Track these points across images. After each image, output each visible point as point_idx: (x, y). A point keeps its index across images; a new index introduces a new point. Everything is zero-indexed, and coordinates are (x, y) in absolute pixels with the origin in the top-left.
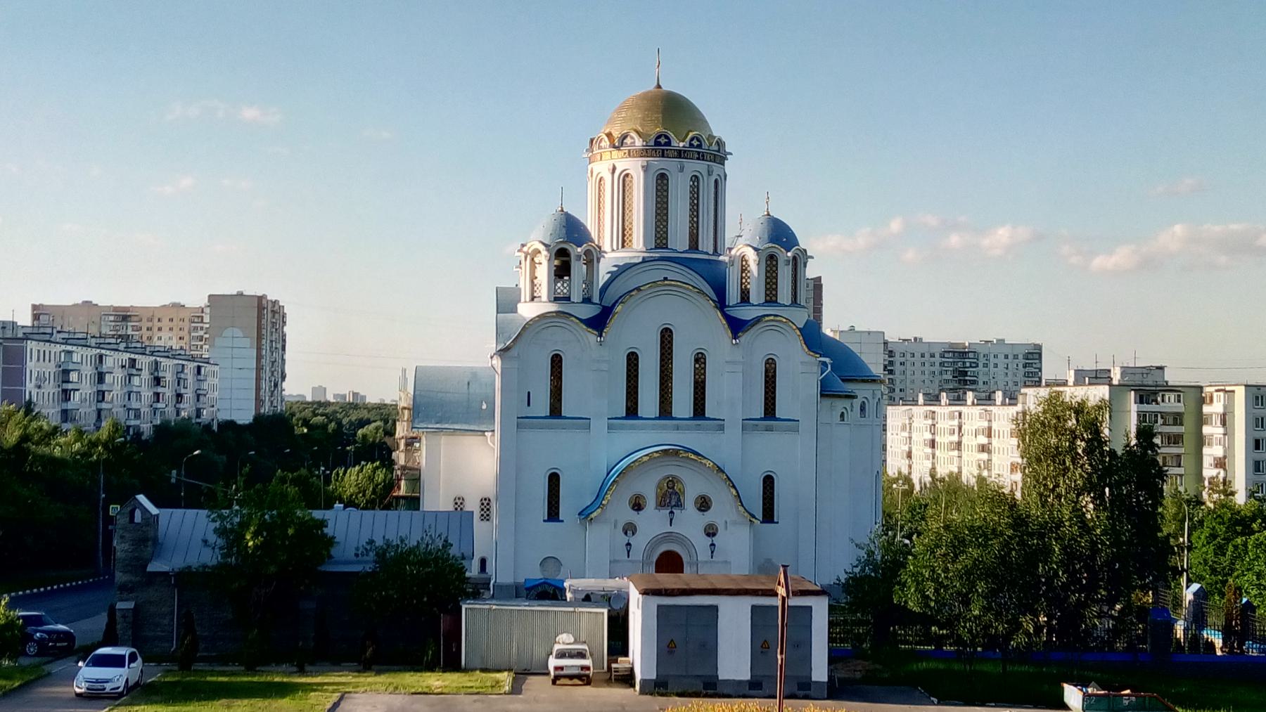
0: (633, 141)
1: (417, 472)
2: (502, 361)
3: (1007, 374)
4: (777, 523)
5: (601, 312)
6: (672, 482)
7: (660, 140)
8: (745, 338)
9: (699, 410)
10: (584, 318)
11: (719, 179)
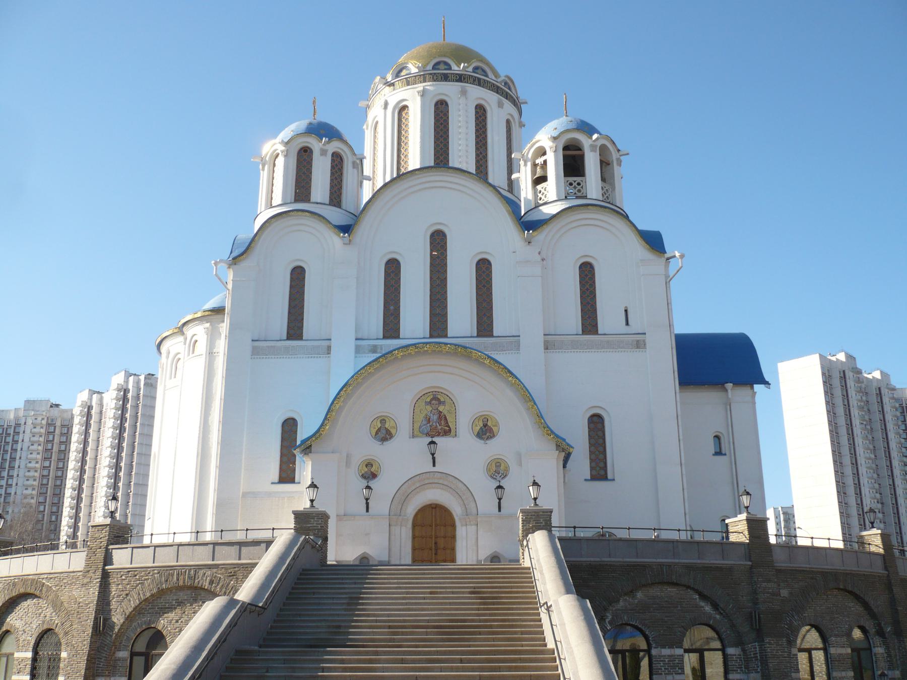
1: (56, 549)
2: (233, 271)
3: (481, 171)
5: (852, 633)
6: (435, 399)
9: (485, 325)
10: (337, 224)
11: (512, 121)
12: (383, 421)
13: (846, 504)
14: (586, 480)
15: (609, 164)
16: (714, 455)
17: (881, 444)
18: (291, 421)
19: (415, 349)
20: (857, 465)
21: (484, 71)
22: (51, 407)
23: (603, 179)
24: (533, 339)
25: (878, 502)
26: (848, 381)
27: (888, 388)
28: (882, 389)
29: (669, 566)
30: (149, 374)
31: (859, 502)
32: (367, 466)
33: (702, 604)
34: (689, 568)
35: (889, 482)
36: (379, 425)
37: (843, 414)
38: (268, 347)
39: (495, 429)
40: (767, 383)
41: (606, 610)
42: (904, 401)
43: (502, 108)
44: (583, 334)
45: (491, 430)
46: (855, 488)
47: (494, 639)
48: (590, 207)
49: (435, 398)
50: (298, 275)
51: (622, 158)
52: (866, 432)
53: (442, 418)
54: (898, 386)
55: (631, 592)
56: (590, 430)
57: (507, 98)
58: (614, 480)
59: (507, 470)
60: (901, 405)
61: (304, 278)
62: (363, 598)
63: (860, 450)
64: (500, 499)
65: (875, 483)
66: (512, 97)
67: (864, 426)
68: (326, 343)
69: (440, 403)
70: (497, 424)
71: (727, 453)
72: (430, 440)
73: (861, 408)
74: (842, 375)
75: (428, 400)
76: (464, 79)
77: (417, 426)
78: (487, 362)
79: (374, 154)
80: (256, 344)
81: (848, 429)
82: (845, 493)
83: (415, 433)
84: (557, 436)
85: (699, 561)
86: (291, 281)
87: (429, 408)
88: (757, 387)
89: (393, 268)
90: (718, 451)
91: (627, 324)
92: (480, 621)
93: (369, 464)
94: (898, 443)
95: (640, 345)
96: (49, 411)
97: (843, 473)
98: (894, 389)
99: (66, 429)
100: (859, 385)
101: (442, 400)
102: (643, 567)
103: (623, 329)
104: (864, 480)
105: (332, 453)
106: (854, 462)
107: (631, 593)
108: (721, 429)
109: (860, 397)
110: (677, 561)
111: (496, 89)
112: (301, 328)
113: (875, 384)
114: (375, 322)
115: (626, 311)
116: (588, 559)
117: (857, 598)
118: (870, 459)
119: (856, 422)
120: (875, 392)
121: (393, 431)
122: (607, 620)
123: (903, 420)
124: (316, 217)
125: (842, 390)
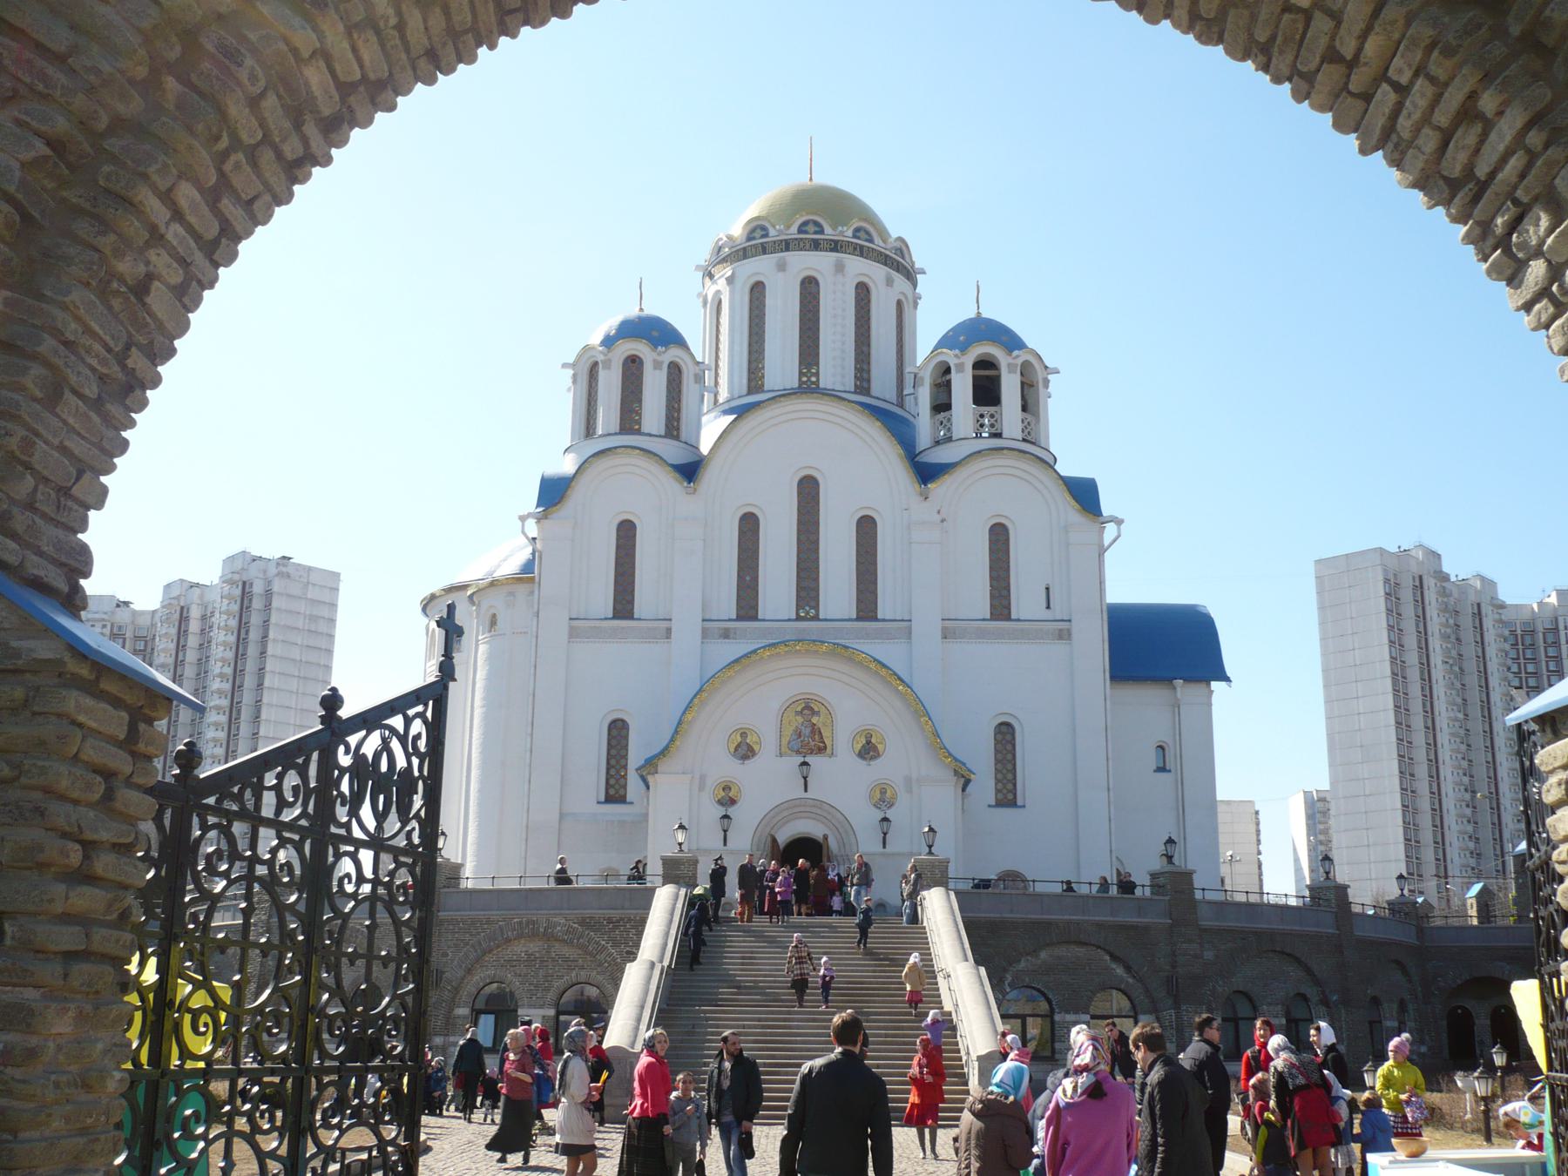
0: (764, 233)
4: (1024, 806)
6: (808, 708)
7: (807, 228)
8: (938, 488)
9: (867, 607)
10: (675, 463)
11: (904, 300)
12: (744, 735)
13: (1412, 792)
14: (989, 806)
15: (1033, 386)
16: (1155, 771)
17: (1475, 696)
18: (620, 723)
19: (779, 646)
20: (1434, 729)
21: (867, 233)
22: (118, 606)
23: (1024, 409)
24: (927, 626)
25: (1466, 790)
26: (1426, 593)
27: (1493, 605)
28: (1483, 606)
29: (1078, 923)
30: (284, 557)
31: (1435, 789)
32: (724, 789)
33: (1114, 966)
34: (1100, 926)
35: (1486, 757)
36: (739, 739)
37: (1415, 646)
38: (591, 627)
39: (880, 747)
40: (1228, 680)
41: (1005, 970)
42: (1518, 626)
43: (892, 286)
44: (991, 619)
45: (875, 748)
46: (1430, 767)
47: (893, 1002)
48: (1005, 452)
49: (807, 707)
50: (626, 533)
51: (1050, 377)
52: (1452, 676)
53: (815, 731)
54: (1509, 601)
55: (1034, 951)
56: (997, 742)
57: (898, 271)
58: (1024, 806)
59: (895, 796)
60: (1513, 632)
61: (635, 535)
62: (724, 947)
63: (1441, 706)
64: (885, 834)
65: (1464, 758)
66: (906, 268)
67: (1448, 667)
68: (665, 624)
69: (814, 713)
70: (883, 741)
71: (1173, 770)
72: (802, 760)
73: (1445, 637)
74: (1417, 584)
75: (799, 709)
76: (841, 247)
77: (785, 742)
78: (872, 666)
79: (717, 345)
80: (575, 623)
81: (1422, 673)
82: (1412, 775)
83: (783, 750)
84: (956, 760)
85: (1112, 919)
86: (617, 540)
87: (800, 719)
88: (1214, 685)
89: (749, 526)
90: (1162, 765)
91: (1048, 607)
92: (877, 983)
93: (727, 788)
94: (1504, 695)
95: (1064, 635)
96: (113, 613)
97: (1411, 743)
98: (1502, 606)
99: (143, 643)
100: (1445, 600)
101: (816, 709)
102: (1049, 924)
103: (1043, 613)
104: (1445, 754)
105: (683, 773)
106: (1430, 724)
107: (1035, 952)
108: (1164, 736)
109: (1444, 620)
110: (1087, 918)
111: (885, 260)
112: (632, 602)
113: (1472, 598)
114: (726, 603)
115: (1047, 589)
116: (988, 915)
117: (1298, 960)
118: (1456, 720)
119: (1437, 659)
120: (1470, 611)
121: (756, 748)
122: (1006, 983)
123: (1515, 657)
124: (652, 456)
125: (1416, 607)
